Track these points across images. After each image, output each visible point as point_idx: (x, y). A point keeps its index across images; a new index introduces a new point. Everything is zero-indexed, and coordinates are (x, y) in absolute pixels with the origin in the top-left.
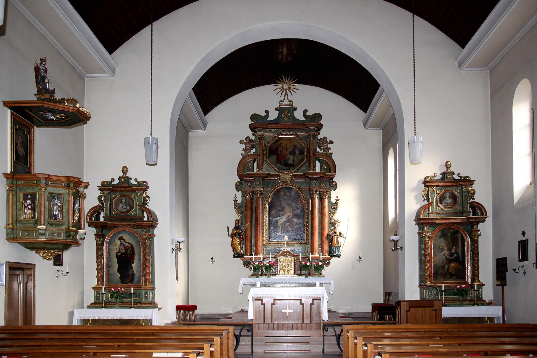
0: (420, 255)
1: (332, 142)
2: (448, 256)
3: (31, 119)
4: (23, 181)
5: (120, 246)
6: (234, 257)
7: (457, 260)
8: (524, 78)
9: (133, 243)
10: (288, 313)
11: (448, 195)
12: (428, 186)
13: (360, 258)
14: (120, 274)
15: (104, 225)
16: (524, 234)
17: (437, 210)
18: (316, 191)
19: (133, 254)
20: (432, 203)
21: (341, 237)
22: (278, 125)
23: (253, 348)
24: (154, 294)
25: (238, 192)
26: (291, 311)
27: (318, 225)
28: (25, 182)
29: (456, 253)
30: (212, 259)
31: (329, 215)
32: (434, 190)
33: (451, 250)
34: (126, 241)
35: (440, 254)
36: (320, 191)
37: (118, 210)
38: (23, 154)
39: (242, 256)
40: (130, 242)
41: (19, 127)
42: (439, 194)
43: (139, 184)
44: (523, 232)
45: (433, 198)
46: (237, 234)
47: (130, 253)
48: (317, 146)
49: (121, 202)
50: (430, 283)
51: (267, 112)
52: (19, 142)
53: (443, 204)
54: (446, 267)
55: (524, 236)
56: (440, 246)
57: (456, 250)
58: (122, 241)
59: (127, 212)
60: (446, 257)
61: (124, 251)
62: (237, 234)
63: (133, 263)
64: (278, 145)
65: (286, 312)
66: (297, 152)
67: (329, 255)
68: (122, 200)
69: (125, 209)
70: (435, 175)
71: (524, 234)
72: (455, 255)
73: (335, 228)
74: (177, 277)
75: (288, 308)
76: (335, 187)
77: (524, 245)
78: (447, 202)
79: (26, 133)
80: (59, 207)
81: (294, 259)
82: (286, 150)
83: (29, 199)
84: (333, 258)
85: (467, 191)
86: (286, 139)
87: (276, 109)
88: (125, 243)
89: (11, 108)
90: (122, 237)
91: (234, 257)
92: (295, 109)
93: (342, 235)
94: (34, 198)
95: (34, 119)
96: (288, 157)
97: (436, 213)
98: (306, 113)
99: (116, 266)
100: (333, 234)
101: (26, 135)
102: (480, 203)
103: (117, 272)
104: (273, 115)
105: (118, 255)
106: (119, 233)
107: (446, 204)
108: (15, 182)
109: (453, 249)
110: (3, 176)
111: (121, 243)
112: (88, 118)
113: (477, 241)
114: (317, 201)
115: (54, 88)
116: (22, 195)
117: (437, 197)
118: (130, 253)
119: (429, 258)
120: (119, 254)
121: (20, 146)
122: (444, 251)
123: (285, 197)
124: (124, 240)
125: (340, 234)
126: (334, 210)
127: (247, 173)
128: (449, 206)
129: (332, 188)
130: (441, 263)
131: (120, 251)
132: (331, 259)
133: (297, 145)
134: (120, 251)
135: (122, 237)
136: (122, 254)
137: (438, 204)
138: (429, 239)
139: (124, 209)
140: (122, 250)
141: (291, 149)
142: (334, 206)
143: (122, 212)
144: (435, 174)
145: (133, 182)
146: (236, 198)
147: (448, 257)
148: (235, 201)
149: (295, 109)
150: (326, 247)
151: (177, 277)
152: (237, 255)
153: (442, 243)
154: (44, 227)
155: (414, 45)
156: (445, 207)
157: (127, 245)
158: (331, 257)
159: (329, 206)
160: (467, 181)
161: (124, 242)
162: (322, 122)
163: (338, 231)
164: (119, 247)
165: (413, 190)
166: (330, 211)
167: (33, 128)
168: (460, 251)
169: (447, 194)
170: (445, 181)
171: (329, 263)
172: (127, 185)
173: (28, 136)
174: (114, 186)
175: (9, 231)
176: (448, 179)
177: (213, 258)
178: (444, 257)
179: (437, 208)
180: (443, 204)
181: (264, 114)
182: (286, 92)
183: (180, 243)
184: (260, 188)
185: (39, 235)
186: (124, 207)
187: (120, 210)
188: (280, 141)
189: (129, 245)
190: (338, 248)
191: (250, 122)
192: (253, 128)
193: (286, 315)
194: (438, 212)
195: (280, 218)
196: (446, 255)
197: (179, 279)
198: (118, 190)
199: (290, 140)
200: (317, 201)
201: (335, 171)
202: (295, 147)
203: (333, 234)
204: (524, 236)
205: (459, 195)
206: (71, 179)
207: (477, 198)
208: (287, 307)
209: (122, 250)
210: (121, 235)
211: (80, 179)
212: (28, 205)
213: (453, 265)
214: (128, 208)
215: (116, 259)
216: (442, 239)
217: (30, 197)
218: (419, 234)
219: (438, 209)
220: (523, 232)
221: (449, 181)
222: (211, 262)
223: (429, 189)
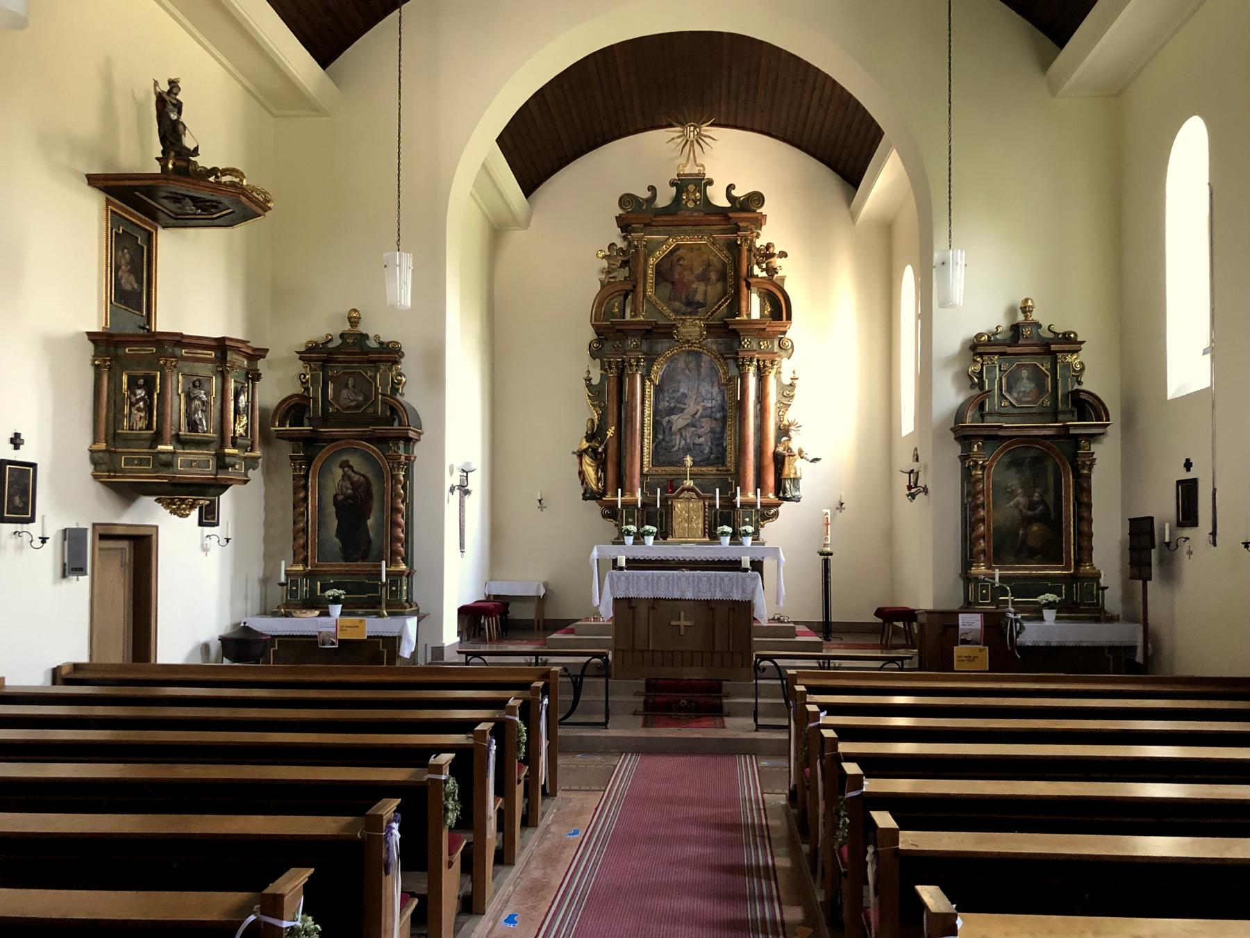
0: (964, 506)
1: (783, 255)
2: (1024, 508)
3: (152, 214)
4: (128, 347)
5: (343, 479)
6: (583, 499)
7: (1043, 518)
8: (1192, 116)
9: (370, 476)
10: (682, 628)
11: (1025, 373)
12: (981, 355)
13: (842, 504)
14: (341, 540)
15: (309, 436)
16: (1188, 465)
17: (1001, 406)
18: (751, 360)
19: (369, 496)
20: (991, 391)
21: (802, 458)
22: (676, 219)
23: (608, 709)
24: (410, 585)
25: (594, 359)
26: (688, 623)
27: (755, 432)
28: (132, 350)
29: (1042, 501)
30: (540, 501)
31: (778, 410)
32: (994, 363)
33: (1033, 496)
34: (355, 469)
35: (1008, 503)
36: (758, 361)
37: (338, 404)
38: (133, 286)
39: (598, 497)
40: (362, 472)
41: (123, 230)
42: (1006, 371)
43: (384, 349)
44: (1188, 460)
45: (992, 381)
46: (590, 450)
47: (363, 496)
48: (755, 262)
49: (347, 386)
50: (987, 569)
51: (652, 189)
52: (123, 262)
53: (1015, 395)
54: (1021, 532)
55: (1188, 470)
56: (1006, 488)
57: (1041, 496)
58: (346, 469)
59: (358, 407)
60: (1021, 511)
61: (350, 491)
62: (590, 450)
63: (369, 518)
64: (675, 261)
65: (679, 626)
66: (713, 276)
67: (777, 494)
68: (348, 380)
69: (354, 400)
70: (997, 330)
71: (1188, 465)
72: (1041, 507)
73: (790, 439)
74: (462, 545)
75: (682, 619)
76: (791, 350)
77: (1188, 490)
78: (1024, 389)
79: (139, 242)
80: (203, 402)
81: (705, 505)
82: (692, 271)
83: (140, 387)
84: (785, 502)
85: (1068, 366)
86: (692, 248)
87: (672, 184)
88: (353, 474)
89: (106, 190)
90: (348, 461)
91: (583, 499)
92: (710, 182)
93: (803, 454)
94: (149, 385)
95: (160, 214)
96: (694, 286)
97: (1000, 414)
98: (732, 191)
99: (334, 524)
100: (785, 452)
101: (140, 246)
102: (1147, 588)
103: (336, 536)
104: (665, 198)
105: (337, 500)
106: (340, 452)
107: (1021, 395)
108: (112, 349)
109: (1036, 494)
110: (86, 337)
111: (345, 475)
112: (264, 207)
113: (1089, 477)
114: (752, 382)
115: (198, 146)
116: (125, 378)
117: (1001, 379)
118: (363, 496)
119: (981, 499)
120: (341, 497)
121: (127, 269)
122: (1017, 498)
123: (688, 373)
124: (351, 467)
125: (800, 452)
126: (787, 399)
127: (611, 322)
128: (1027, 399)
129: (783, 353)
130: (1009, 523)
131: (342, 490)
132: (780, 506)
133: (712, 260)
134: (342, 490)
135: (348, 461)
136: (347, 498)
137: (1003, 392)
138: (983, 472)
139: (352, 401)
140: (347, 489)
141: (701, 269)
142: (788, 392)
143: (348, 408)
144: (997, 328)
145: (372, 344)
146: (589, 373)
147: (1024, 511)
148: (588, 380)
149: (710, 182)
150: (771, 480)
151: (462, 545)
152: (589, 495)
153: (1013, 480)
154: (170, 448)
155: (950, 30)
156: (1019, 401)
157: (356, 478)
158: (781, 502)
159: (778, 393)
160: (1070, 342)
161: (350, 472)
162: (763, 210)
163: (795, 446)
164: (340, 484)
165: (948, 362)
166: (779, 402)
167: (156, 231)
168: (1050, 499)
169: (1024, 371)
170: (1020, 342)
171: (776, 515)
172: (357, 350)
173: (143, 248)
174: (331, 352)
175: (99, 457)
176: (1026, 337)
177: (542, 499)
178: (1016, 513)
179: (1001, 403)
180: (1015, 395)
181: (646, 194)
182: (692, 145)
183: (467, 473)
184: (637, 353)
185: (161, 465)
186: (351, 398)
187: (343, 402)
188: (677, 253)
189: (362, 478)
190: (795, 481)
191: (620, 211)
192: (625, 225)
193: (679, 632)
194: (1002, 411)
195: (677, 417)
196: (1021, 507)
197: (465, 550)
198: (339, 360)
199: (699, 249)
200: (752, 382)
201: (789, 318)
202: (709, 265)
203: (785, 452)
204: (1188, 470)
205: (1049, 374)
206: (228, 343)
207: (1090, 383)
208: (682, 614)
209: (347, 489)
210: (344, 458)
211: (249, 342)
212: (138, 401)
213: (1035, 528)
214: (361, 398)
215: (333, 509)
216: (1013, 472)
217: (142, 383)
218: (963, 459)
219: (1003, 405)
220: (1188, 460)
221: (1029, 342)
222: (539, 507)
223: (983, 361)
